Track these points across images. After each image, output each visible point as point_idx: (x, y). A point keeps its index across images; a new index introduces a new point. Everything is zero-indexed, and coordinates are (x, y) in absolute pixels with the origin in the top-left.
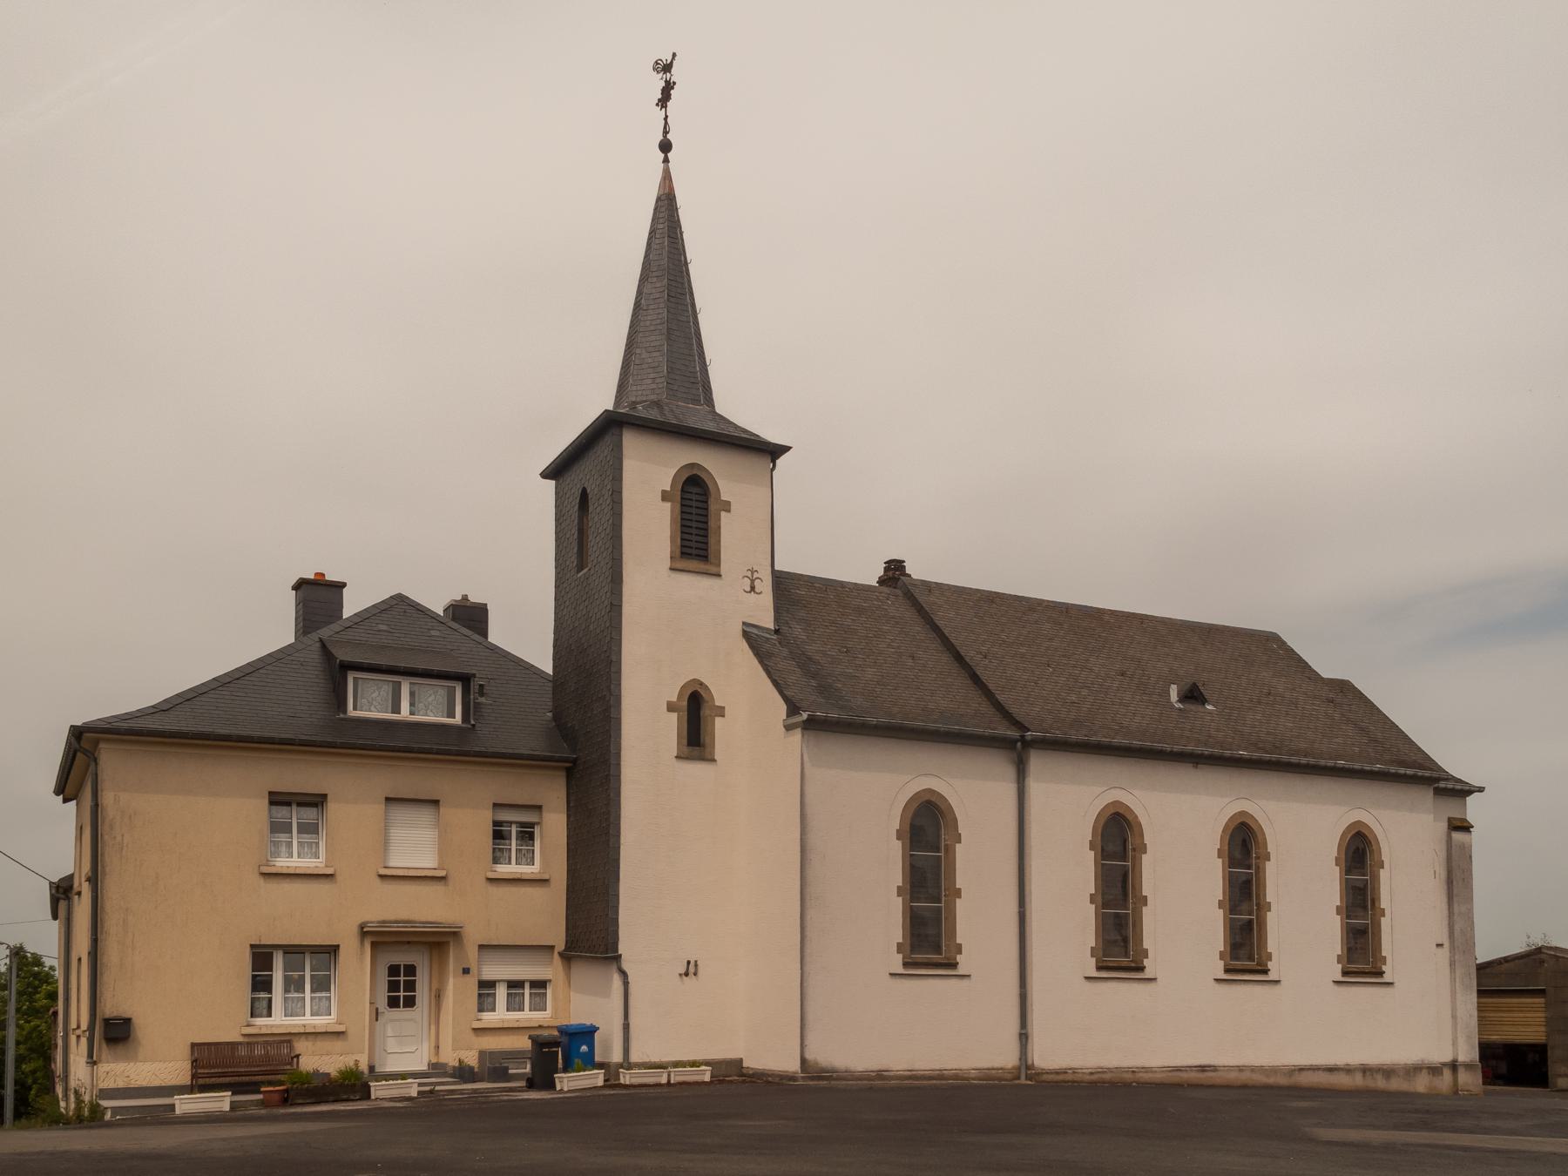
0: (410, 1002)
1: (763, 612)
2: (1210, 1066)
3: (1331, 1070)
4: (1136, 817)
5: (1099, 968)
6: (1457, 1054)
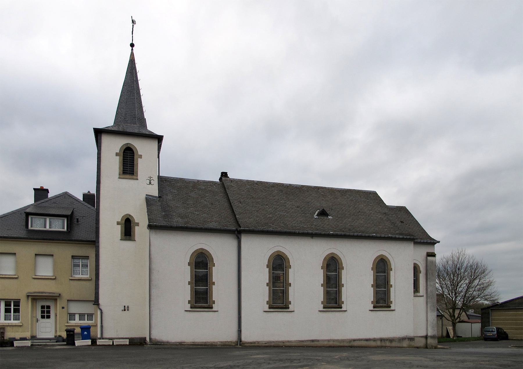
0: (48, 317)
1: (154, 191)
3: (367, 340)
5: (270, 308)
6: (428, 333)
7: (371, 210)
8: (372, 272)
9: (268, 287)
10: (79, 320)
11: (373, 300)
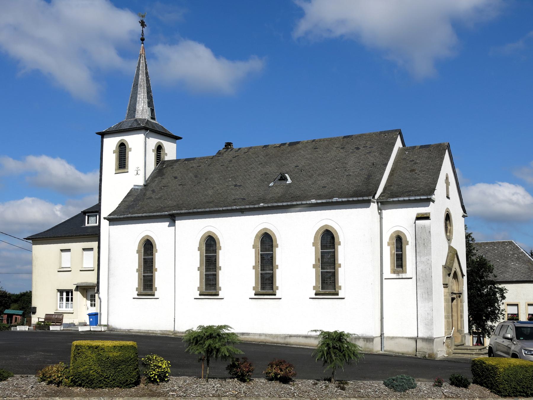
4: (217, 236)
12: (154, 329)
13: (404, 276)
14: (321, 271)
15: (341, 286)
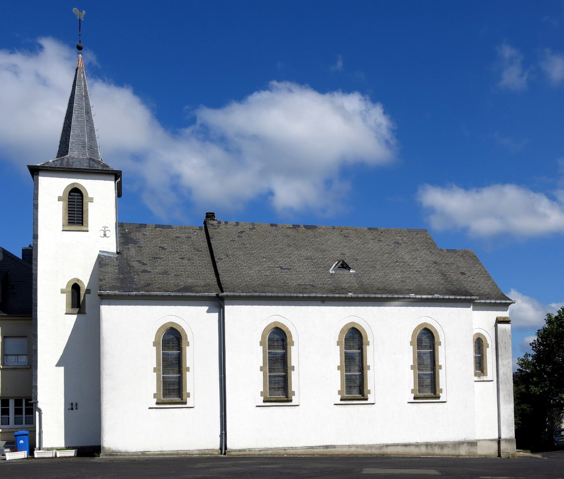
2: (331, 446)
3: (406, 445)
4: (288, 328)
7: (415, 258)
8: (411, 347)
9: (262, 372)
10: (15, 424)
11: (413, 388)
12: (187, 449)
13: (485, 378)
14: (268, 374)
15: (442, 389)
